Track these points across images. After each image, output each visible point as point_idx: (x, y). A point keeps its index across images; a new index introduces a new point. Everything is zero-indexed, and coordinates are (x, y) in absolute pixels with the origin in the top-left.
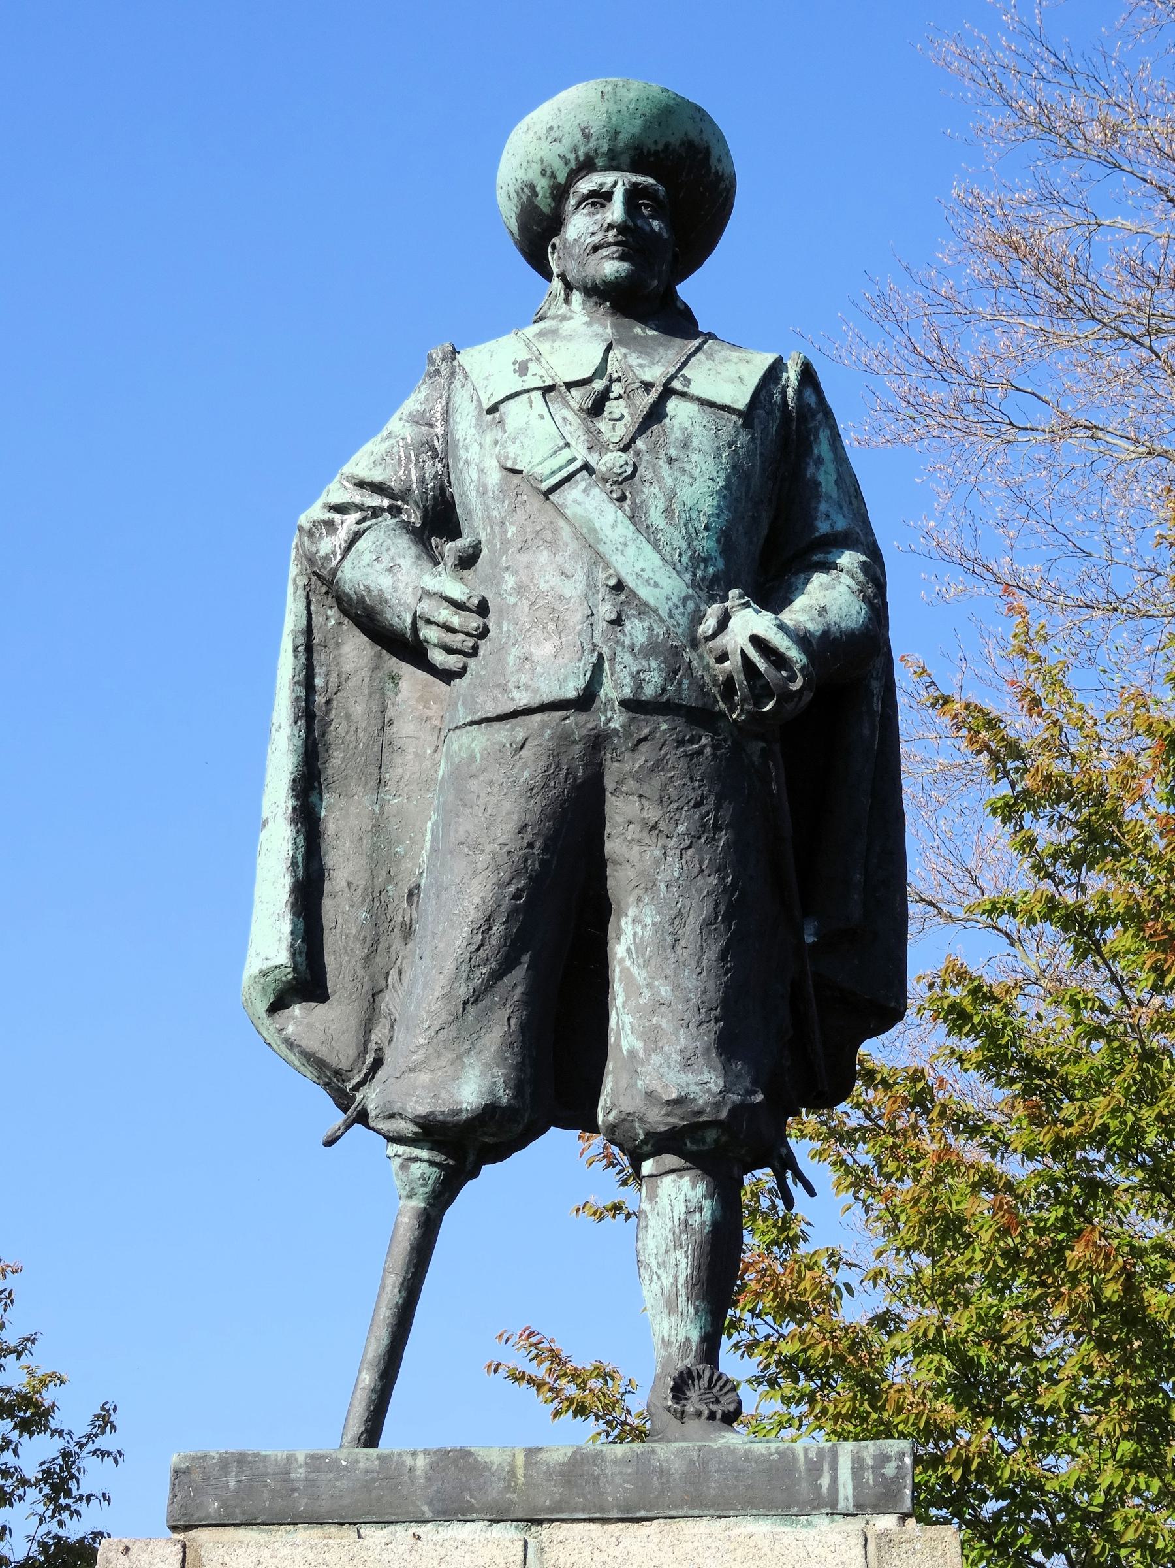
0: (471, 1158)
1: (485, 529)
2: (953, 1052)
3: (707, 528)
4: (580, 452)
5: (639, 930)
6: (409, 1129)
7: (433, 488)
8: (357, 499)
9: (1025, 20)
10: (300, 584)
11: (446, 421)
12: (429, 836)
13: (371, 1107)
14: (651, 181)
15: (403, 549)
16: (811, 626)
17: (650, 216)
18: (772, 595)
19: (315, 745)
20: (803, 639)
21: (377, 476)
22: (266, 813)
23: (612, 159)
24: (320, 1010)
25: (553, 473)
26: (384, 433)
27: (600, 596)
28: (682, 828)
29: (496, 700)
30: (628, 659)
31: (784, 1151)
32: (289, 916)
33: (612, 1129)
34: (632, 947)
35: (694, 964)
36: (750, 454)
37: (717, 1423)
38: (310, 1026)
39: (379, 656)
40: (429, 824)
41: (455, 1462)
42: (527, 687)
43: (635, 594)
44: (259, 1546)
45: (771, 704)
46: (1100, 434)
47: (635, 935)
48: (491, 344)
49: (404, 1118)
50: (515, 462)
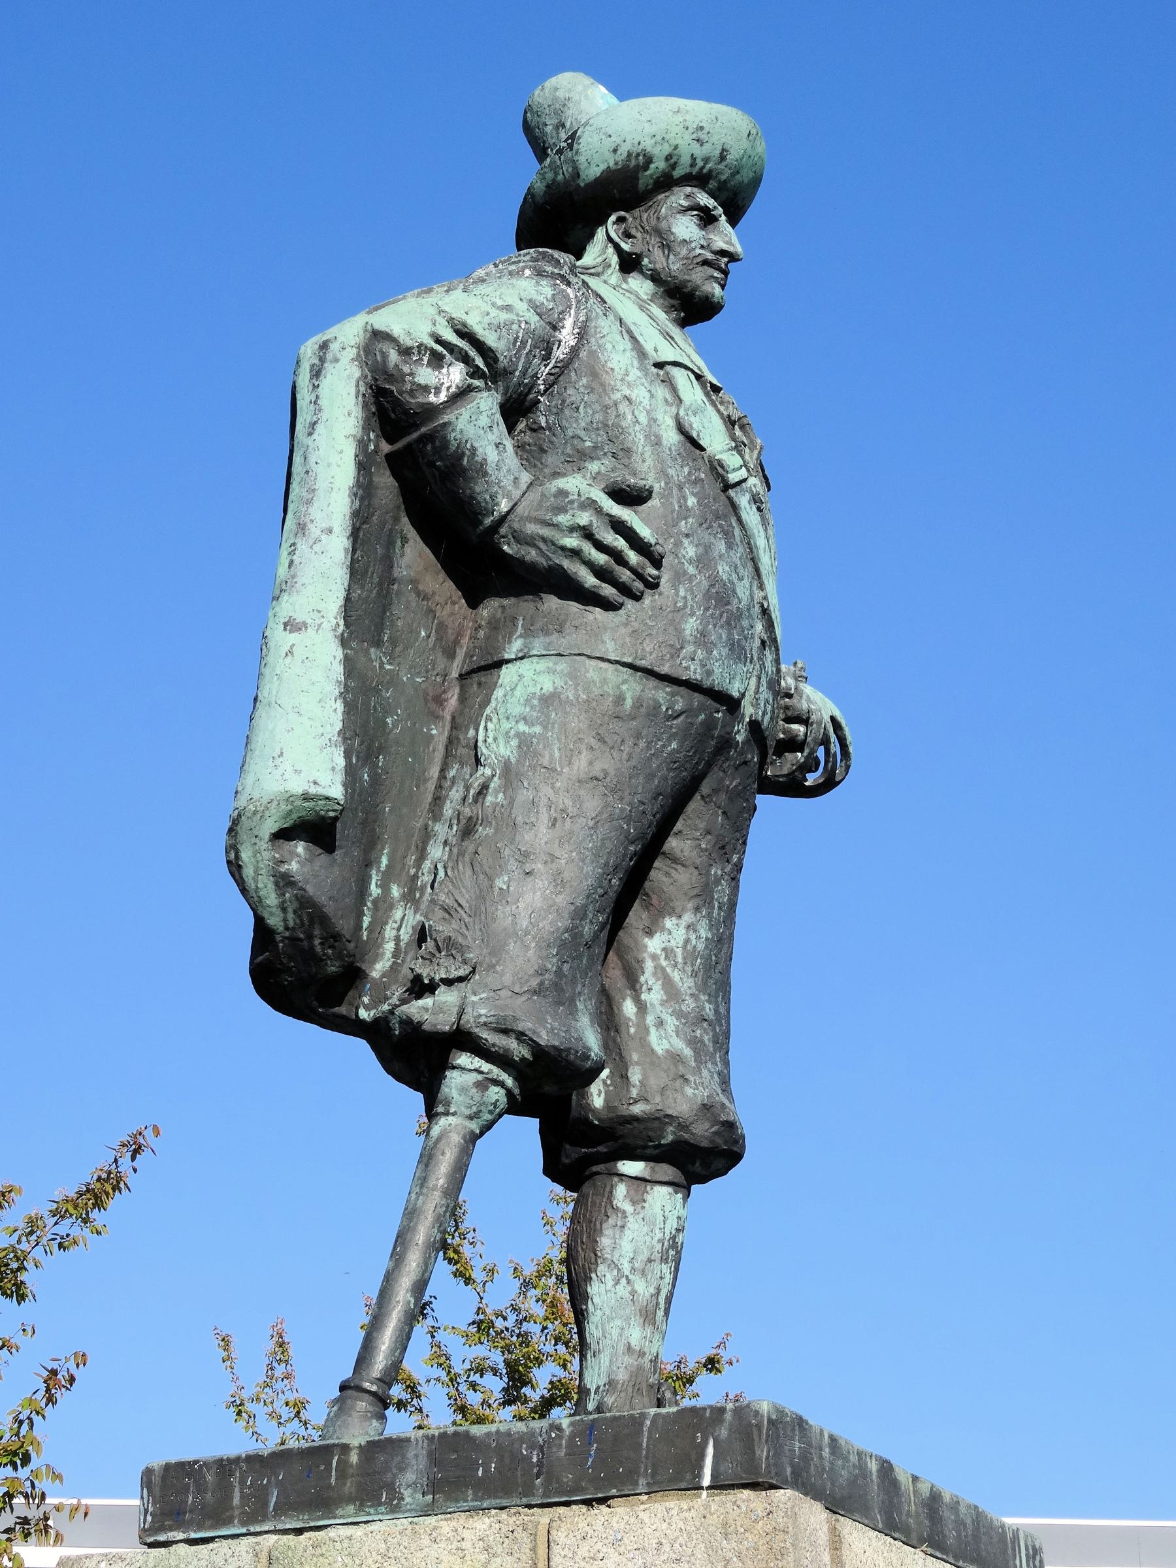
1: (657, 480)
5: (693, 937)
6: (519, 1051)
21: (490, 339)
34: (679, 952)
39: (398, 508)
47: (687, 941)
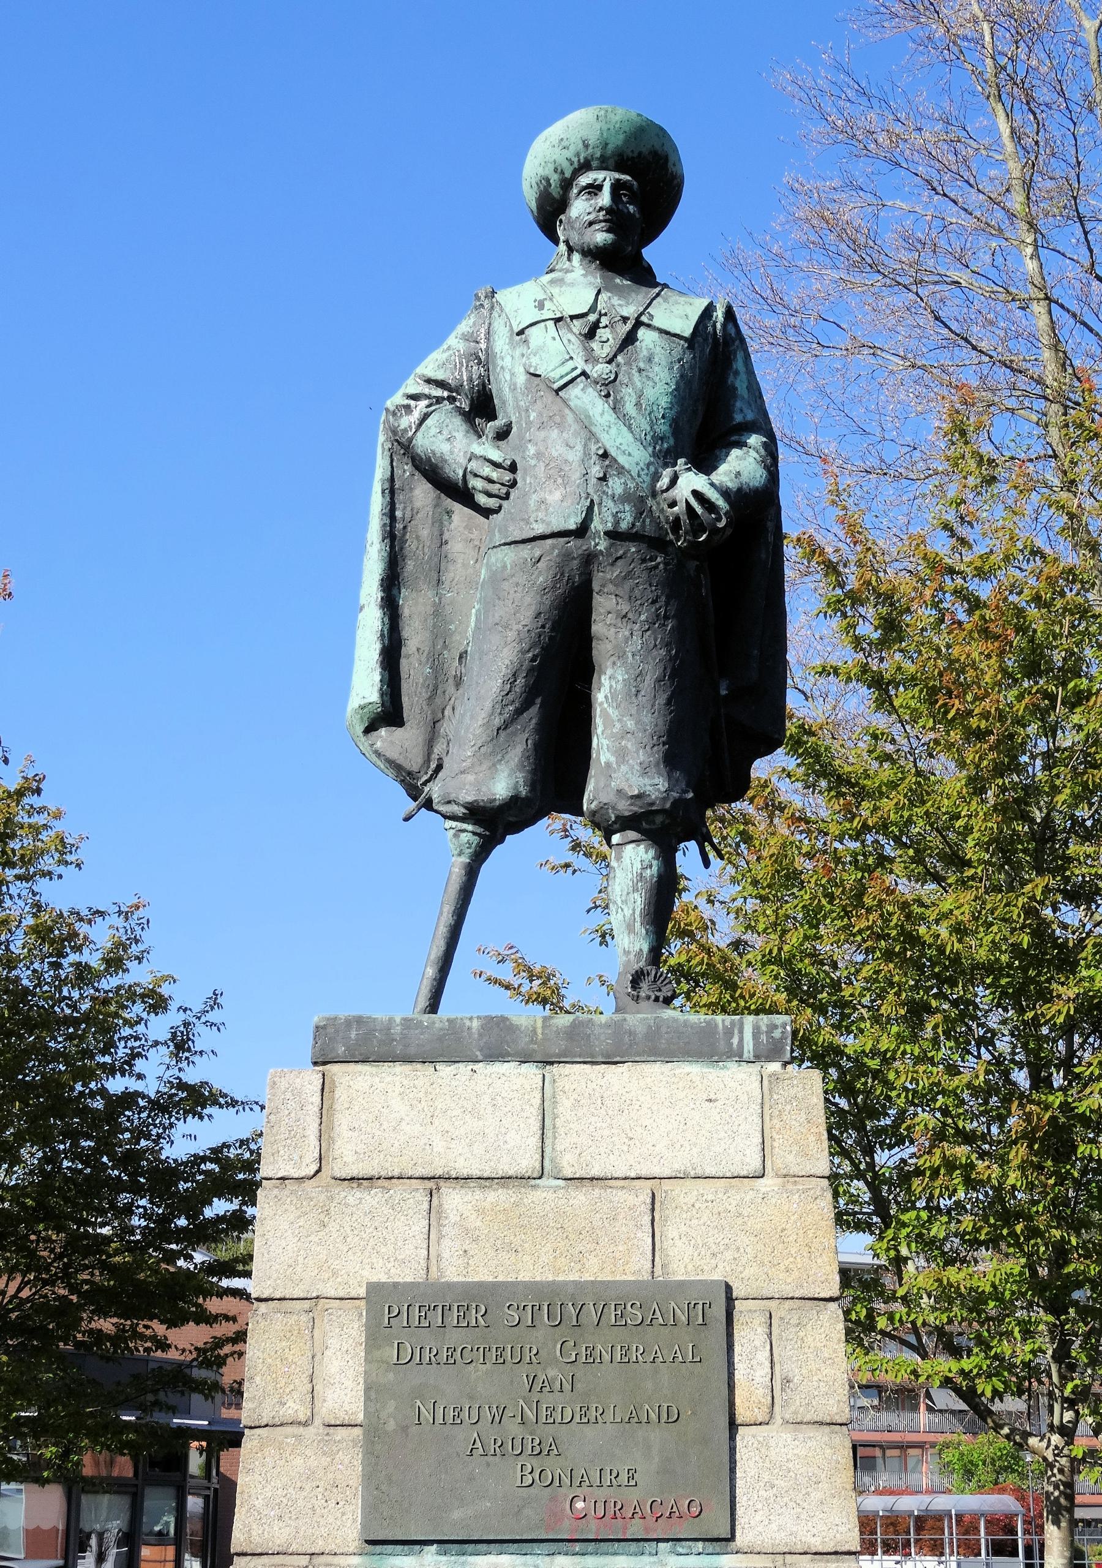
0: (500, 831)
2: (784, 770)
3: (663, 417)
4: (580, 364)
6: (460, 811)
7: (478, 385)
8: (426, 391)
9: (838, 59)
10: (386, 448)
11: (488, 339)
12: (473, 618)
13: (435, 797)
14: (629, 178)
15: (458, 425)
16: (730, 485)
17: (628, 203)
18: (705, 464)
19: (396, 557)
20: (725, 493)
21: (440, 375)
22: (363, 600)
23: (603, 162)
24: (399, 732)
25: (562, 377)
26: (445, 346)
27: (592, 461)
28: (643, 617)
29: (521, 529)
30: (610, 504)
31: (704, 830)
32: (379, 670)
33: (594, 813)
35: (649, 707)
36: (692, 368)
37: (660, 1003)
38: (392, 742)
40: (474, 611)
41: (498, 1024)
42: (543, 521)
43: (616, 460)
44: (371, 1075)
45: (704, 536)
46: (879, 352)
47: (611, 687)
48: (517, 288)
49: (457, 804)
50: (536, 369)
